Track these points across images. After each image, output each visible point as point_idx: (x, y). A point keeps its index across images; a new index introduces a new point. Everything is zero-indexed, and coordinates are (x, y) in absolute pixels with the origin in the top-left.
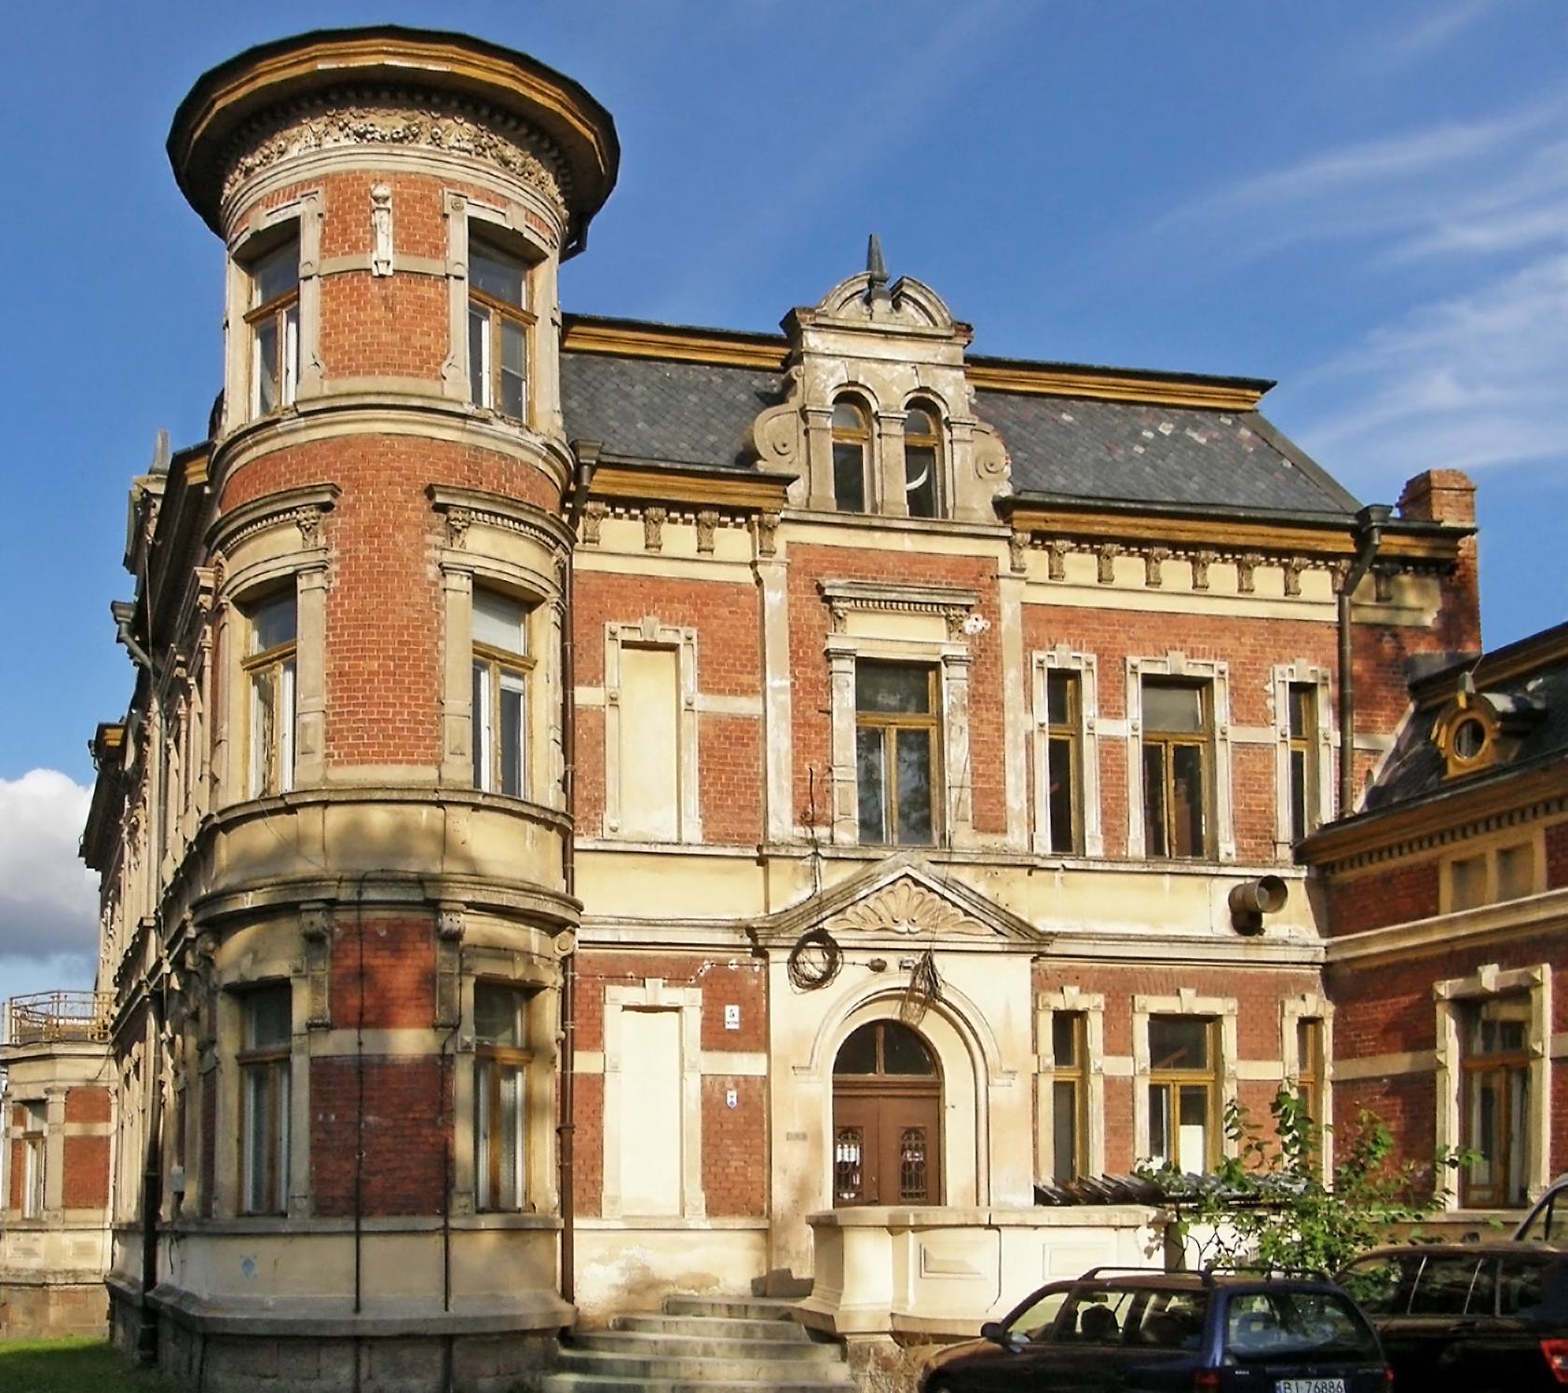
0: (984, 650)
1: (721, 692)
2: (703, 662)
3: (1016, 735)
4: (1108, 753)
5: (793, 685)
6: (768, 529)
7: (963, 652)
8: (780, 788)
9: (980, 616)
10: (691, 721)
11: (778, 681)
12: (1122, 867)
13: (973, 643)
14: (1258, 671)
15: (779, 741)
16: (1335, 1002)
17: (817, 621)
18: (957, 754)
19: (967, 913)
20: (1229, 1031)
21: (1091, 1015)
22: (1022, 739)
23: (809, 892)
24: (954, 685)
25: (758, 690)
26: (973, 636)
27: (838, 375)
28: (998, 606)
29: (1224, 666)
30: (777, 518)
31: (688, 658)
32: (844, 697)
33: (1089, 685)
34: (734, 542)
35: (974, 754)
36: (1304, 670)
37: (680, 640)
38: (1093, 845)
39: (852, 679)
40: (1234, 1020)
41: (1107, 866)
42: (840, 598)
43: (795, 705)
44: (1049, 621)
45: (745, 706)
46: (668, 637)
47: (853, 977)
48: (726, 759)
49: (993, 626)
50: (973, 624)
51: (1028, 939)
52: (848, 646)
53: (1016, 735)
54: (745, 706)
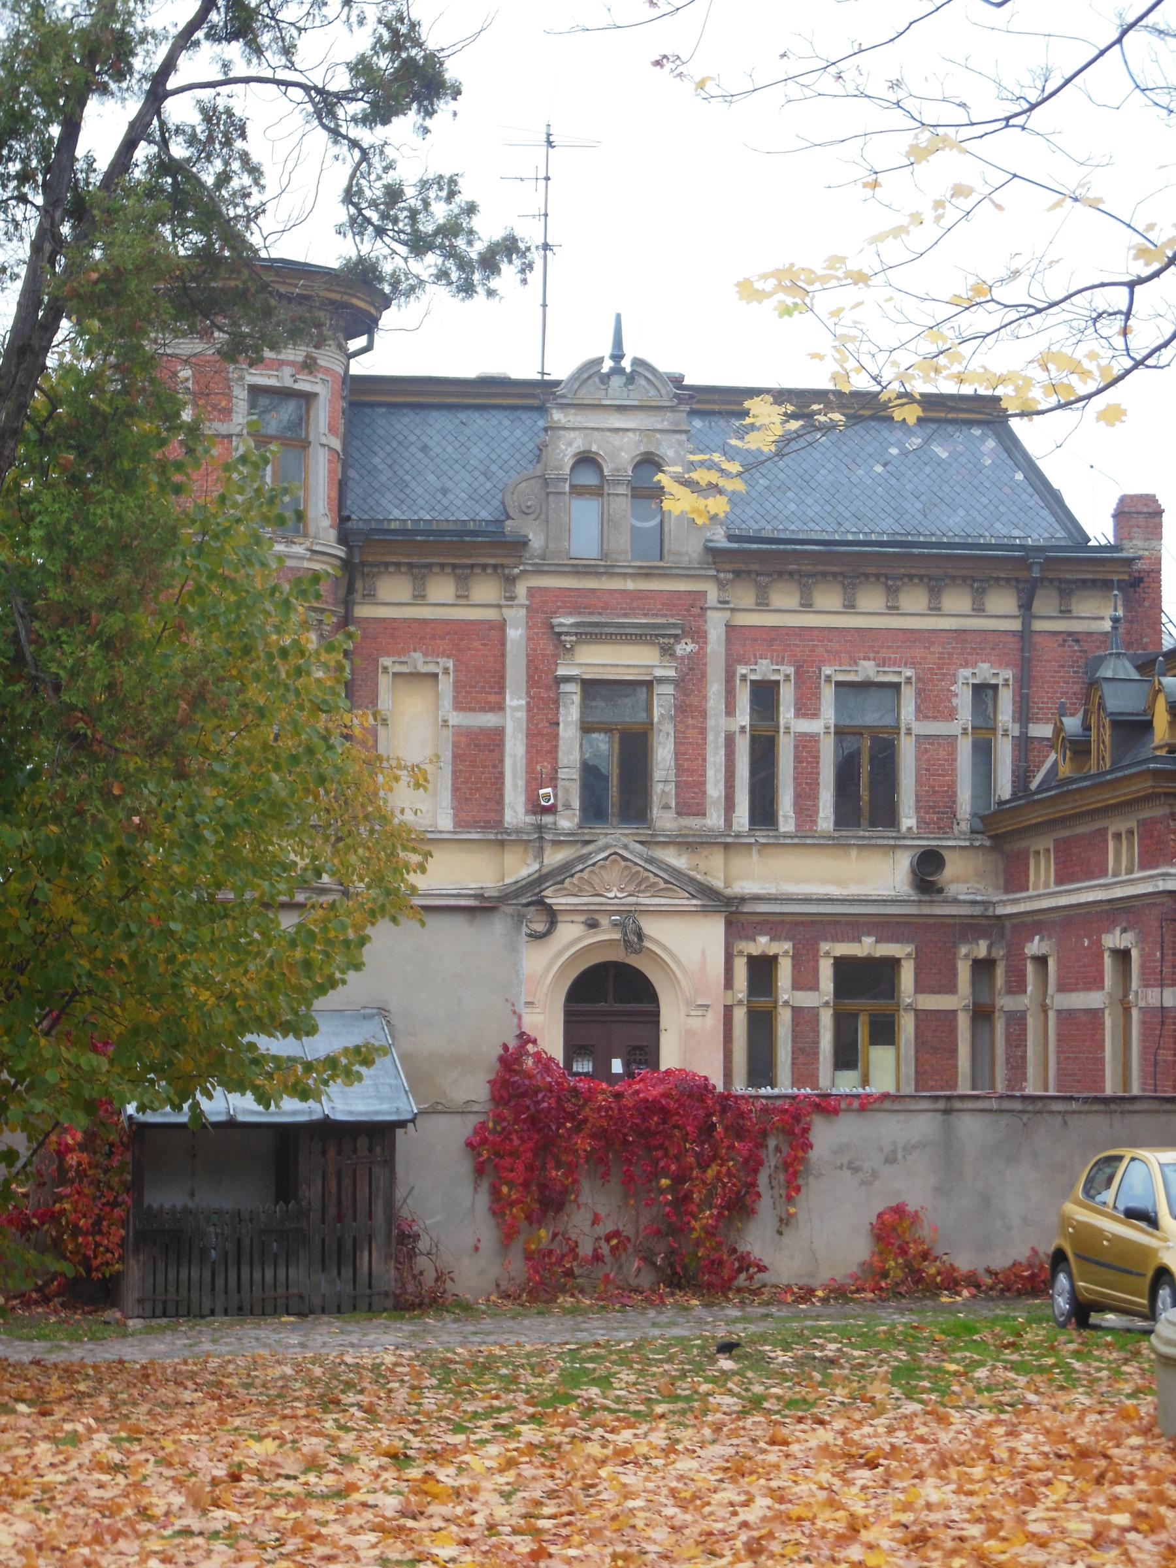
0: (691, 669)
1: (472, 710)
2: (458, 686)
3: (717, 736)
4: (804, 747)
5: (528, 703)
6: (510, 581)
7: (672, 673)
8: (515, 785)
9: (689, 641)
10: (448, 734)
11: (515, 701)
12: (809, 841)
13: (682, 663)
14: (945, 675)
15: (515, 749)
16: (217, 1125)
17: (550, 651)
18: (663, 754)
19: (667, 882)
20: (907, 977)
21: (780, 959)
22: (722, 740)
23: (537, 866)
24: (663, 703)
25: (500, 707)
26: (682, 658)
27: (575, 445)
28: (705, 632)
29: (909, 672)
30: (516, 571)
31: (446, 685)
32: (570, 714)
33: (787, 694)
34: (485, 591)
35: (677, 754)
36: (985, 671)
37: (439, 671)
38: (786, 821)
39: (577, 699)
40: (912, 962)
41: (796, 841)
42: (567, 634)
43: (530, 720)
44: (755, 640)
45: (488, 720)
46: (432, 668)
47: (570, 933)
48: (476, 760)
49: (701, 648)
50: (685, 648)
51: (715, 901)
52: (574, 672)
53: (717, 736)
54: (488, 720)
